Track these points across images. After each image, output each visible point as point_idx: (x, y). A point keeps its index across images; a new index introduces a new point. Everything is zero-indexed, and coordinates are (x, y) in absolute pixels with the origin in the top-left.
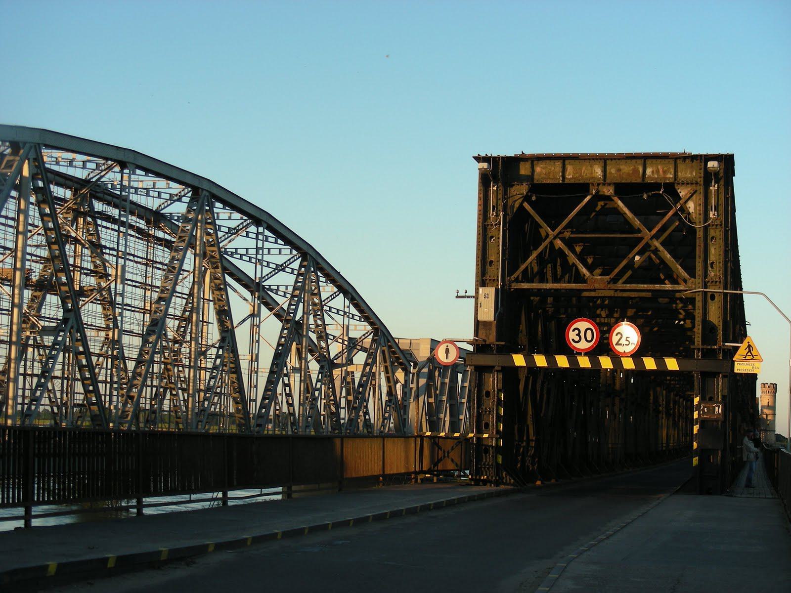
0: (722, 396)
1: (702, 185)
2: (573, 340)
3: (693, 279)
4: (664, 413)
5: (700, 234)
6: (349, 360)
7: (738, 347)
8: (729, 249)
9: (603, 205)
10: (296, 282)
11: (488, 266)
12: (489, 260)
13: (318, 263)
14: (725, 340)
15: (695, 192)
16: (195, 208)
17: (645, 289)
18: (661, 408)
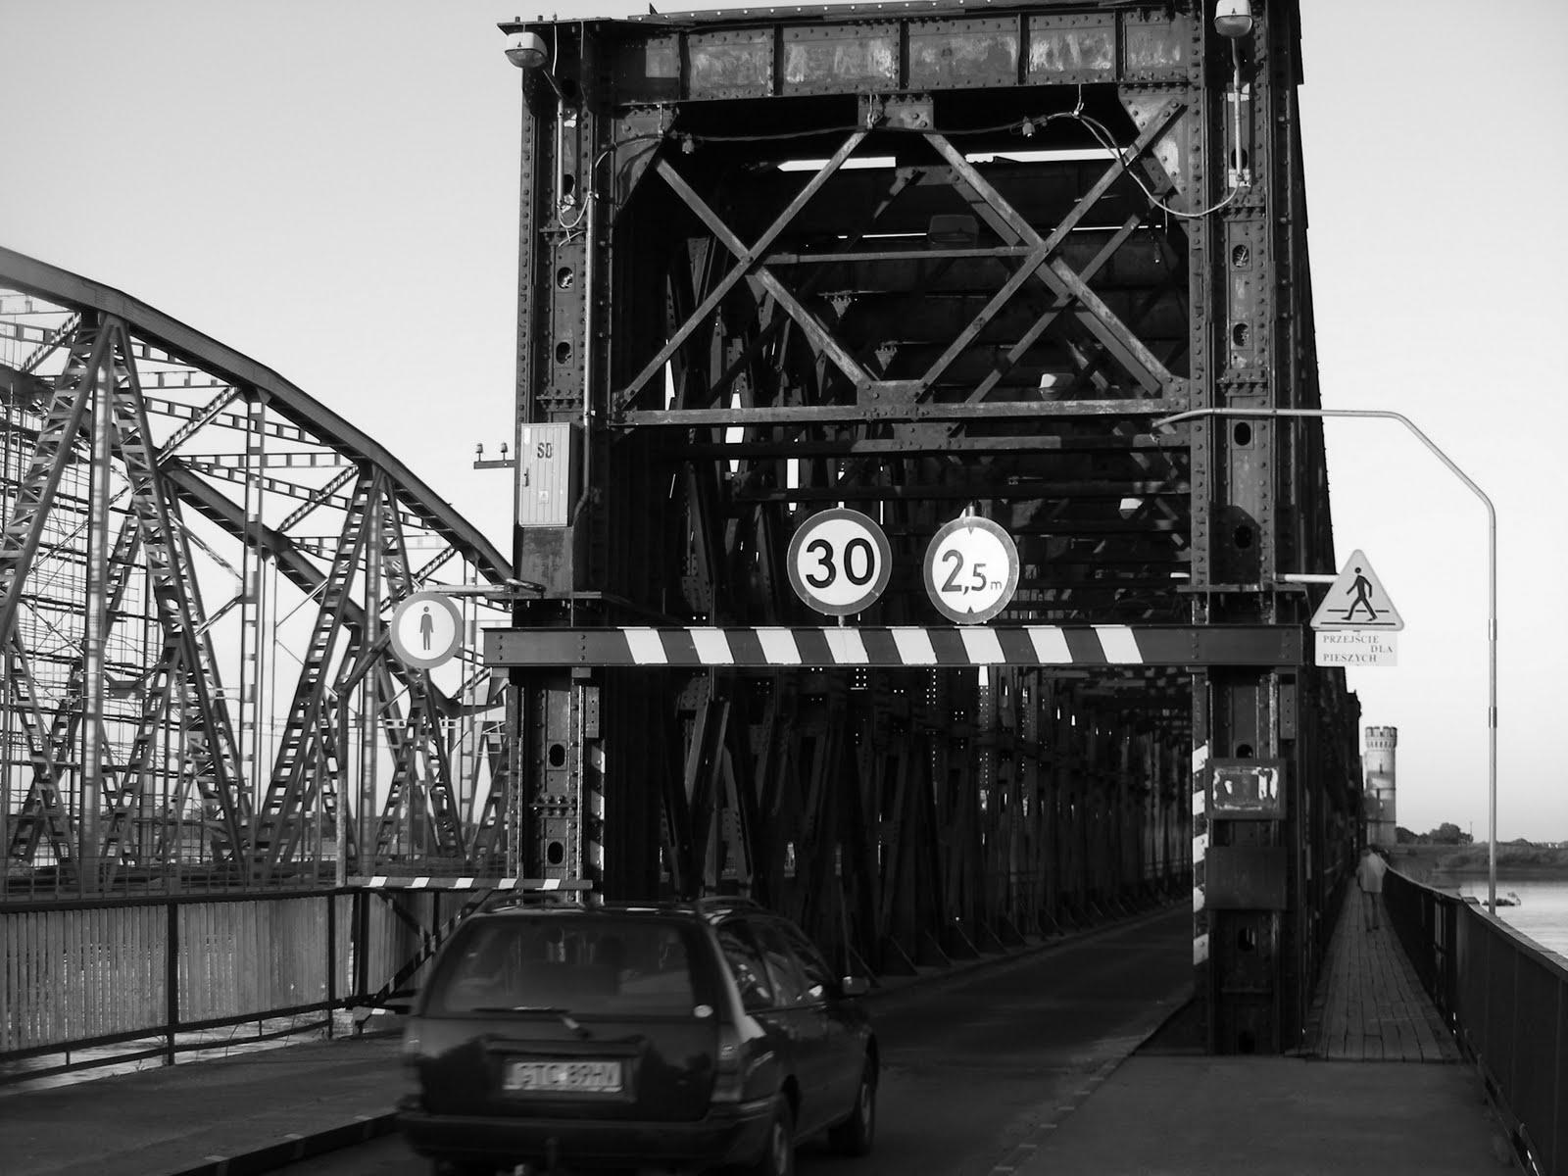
0: (1280, 741)
1: (1202, 85)
2: (810, 578)
3: (1181, 380)
4: (1157, 795)
5: (1198, 238)
6: (496, 698)
7: (1327, 587)
8: (1290, 317)
9: (910, 177)
10: (348, 525)
11: (552, 362)
12: (556, 344)
13: (397, 485)
14: (1285, 565)
15: (1182, 110)
16: (88, 355)
17: (1034, 414)
18: (1148, 784)
